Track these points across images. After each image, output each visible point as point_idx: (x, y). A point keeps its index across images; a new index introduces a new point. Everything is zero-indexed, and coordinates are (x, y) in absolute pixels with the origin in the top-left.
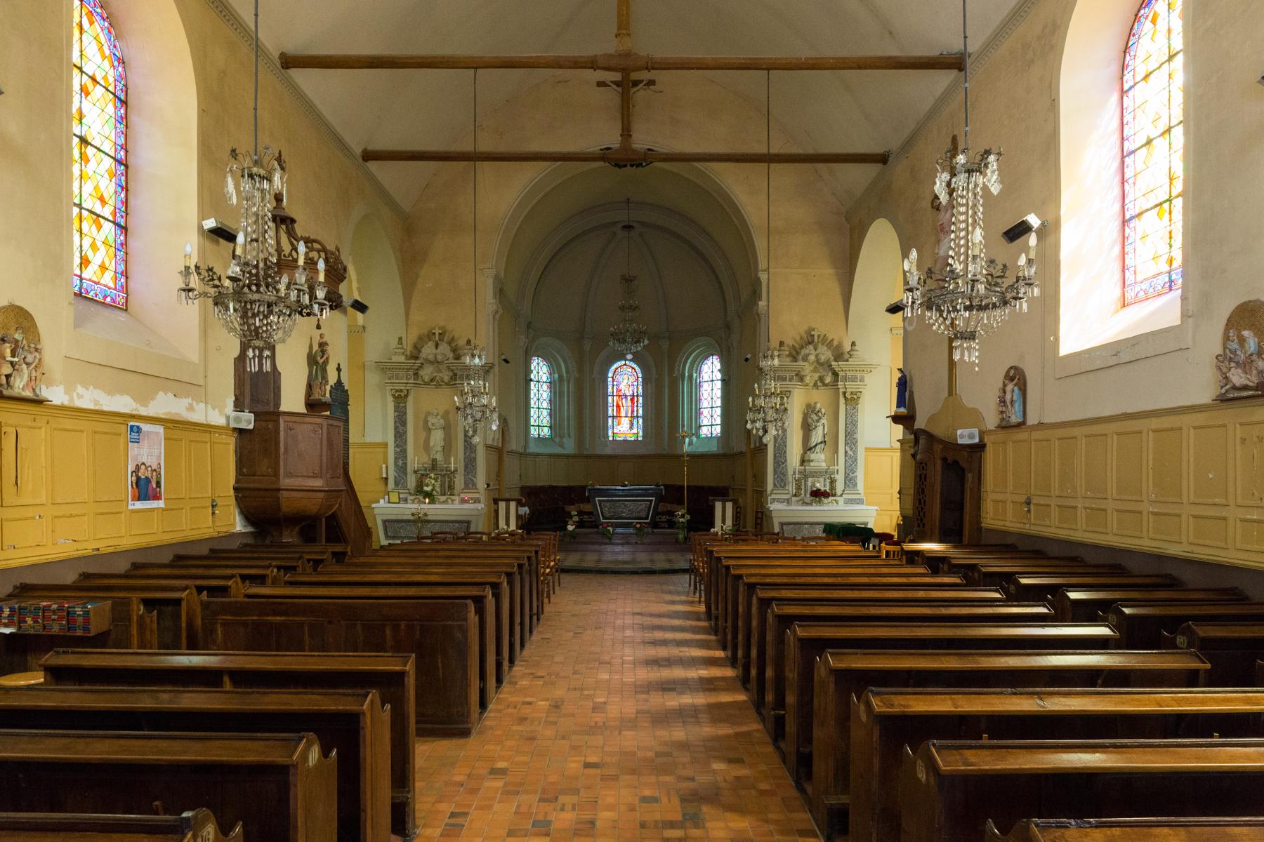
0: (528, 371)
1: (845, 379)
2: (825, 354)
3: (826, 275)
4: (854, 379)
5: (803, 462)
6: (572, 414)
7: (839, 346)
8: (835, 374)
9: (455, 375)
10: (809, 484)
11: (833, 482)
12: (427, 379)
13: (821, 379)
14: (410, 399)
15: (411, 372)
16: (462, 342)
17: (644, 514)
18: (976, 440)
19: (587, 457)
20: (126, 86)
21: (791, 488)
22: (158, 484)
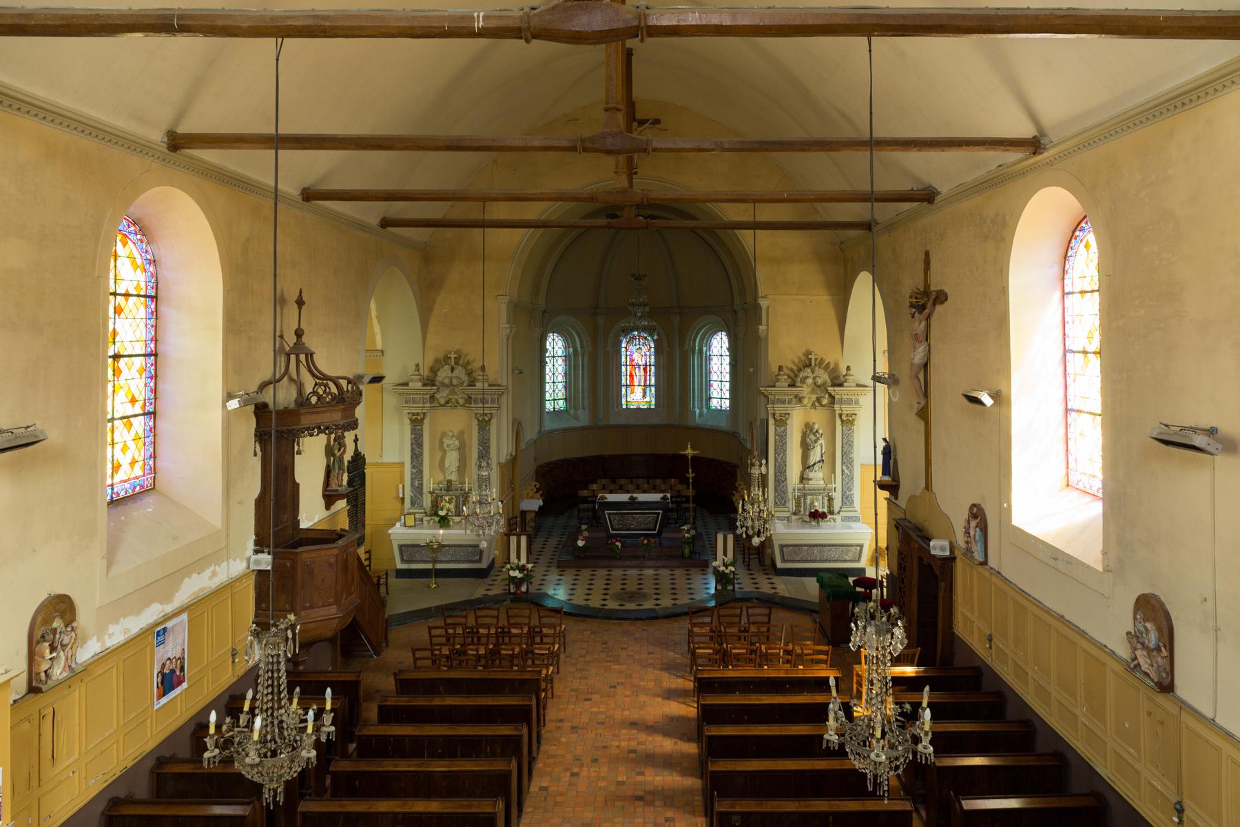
0: (543, 350)
1: (841, 401)
2: (823, 377)
3: (822, 301)
4: (849, 402)
5: (803, 479)
6: (586, 387)
7: (836, 369)
8: (832, 397)
9: (470, 398)
10: (808, 501)
11: (830, 499)
12: (442, 402)
13: (819, 400)
14: (427, 421)
15: (428, 397)
16: (477, 365)
17: (651, 526)
18: (948, 553)
19: (601, 428)
20: (157, 282)
21: (791, 505)
22: (182, 669)
